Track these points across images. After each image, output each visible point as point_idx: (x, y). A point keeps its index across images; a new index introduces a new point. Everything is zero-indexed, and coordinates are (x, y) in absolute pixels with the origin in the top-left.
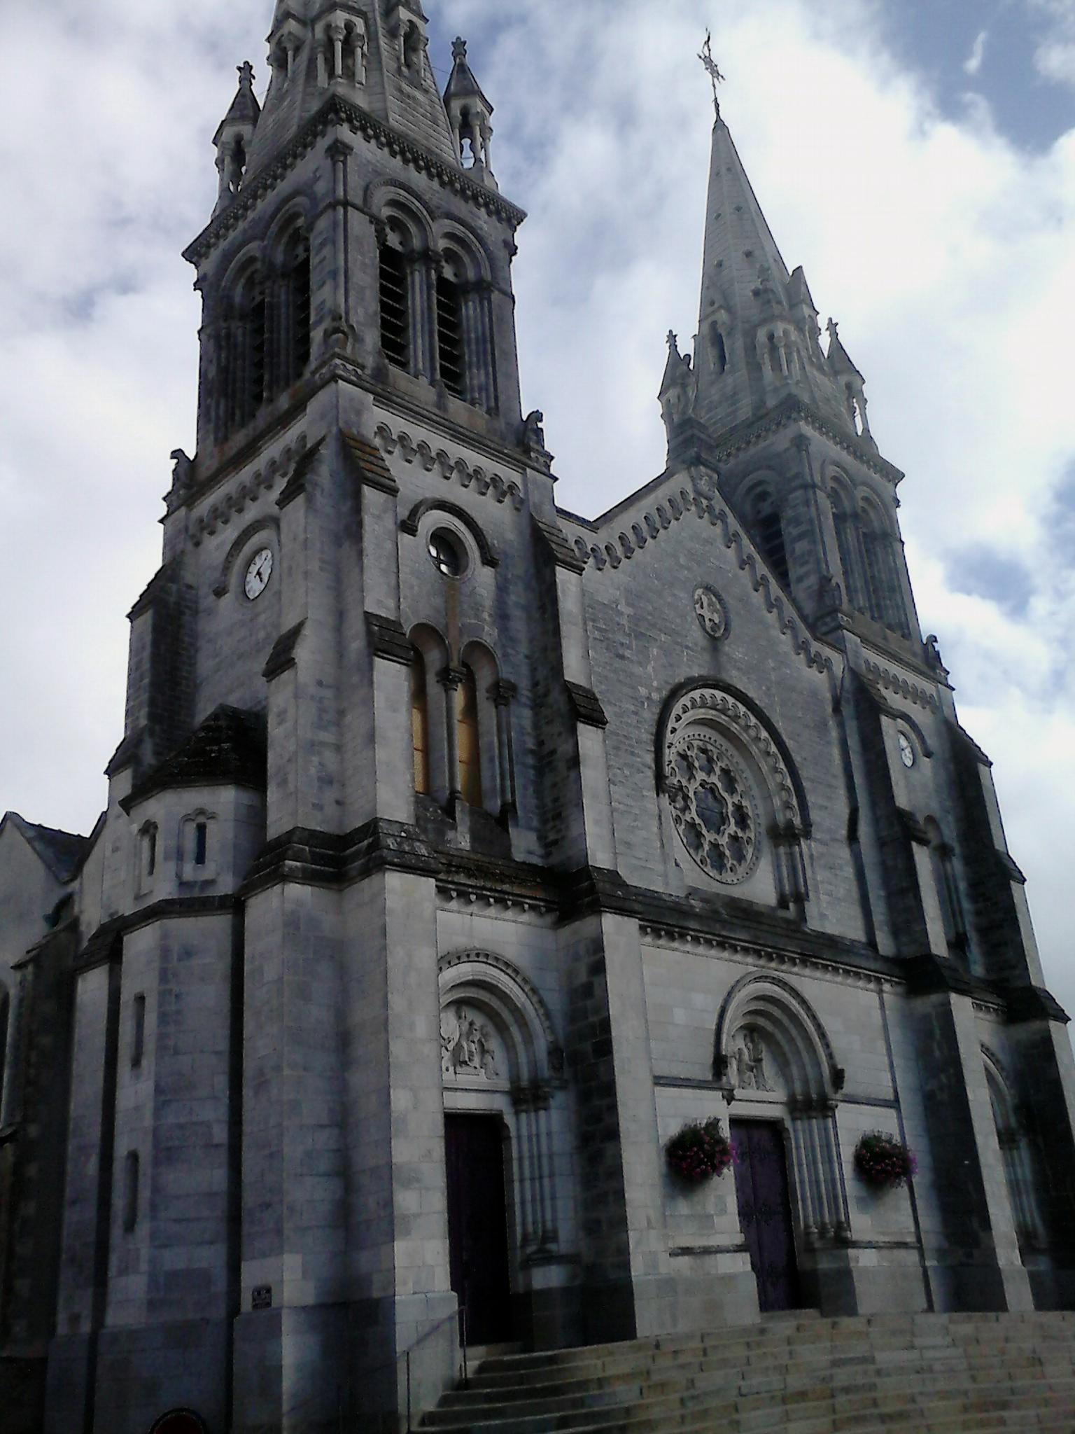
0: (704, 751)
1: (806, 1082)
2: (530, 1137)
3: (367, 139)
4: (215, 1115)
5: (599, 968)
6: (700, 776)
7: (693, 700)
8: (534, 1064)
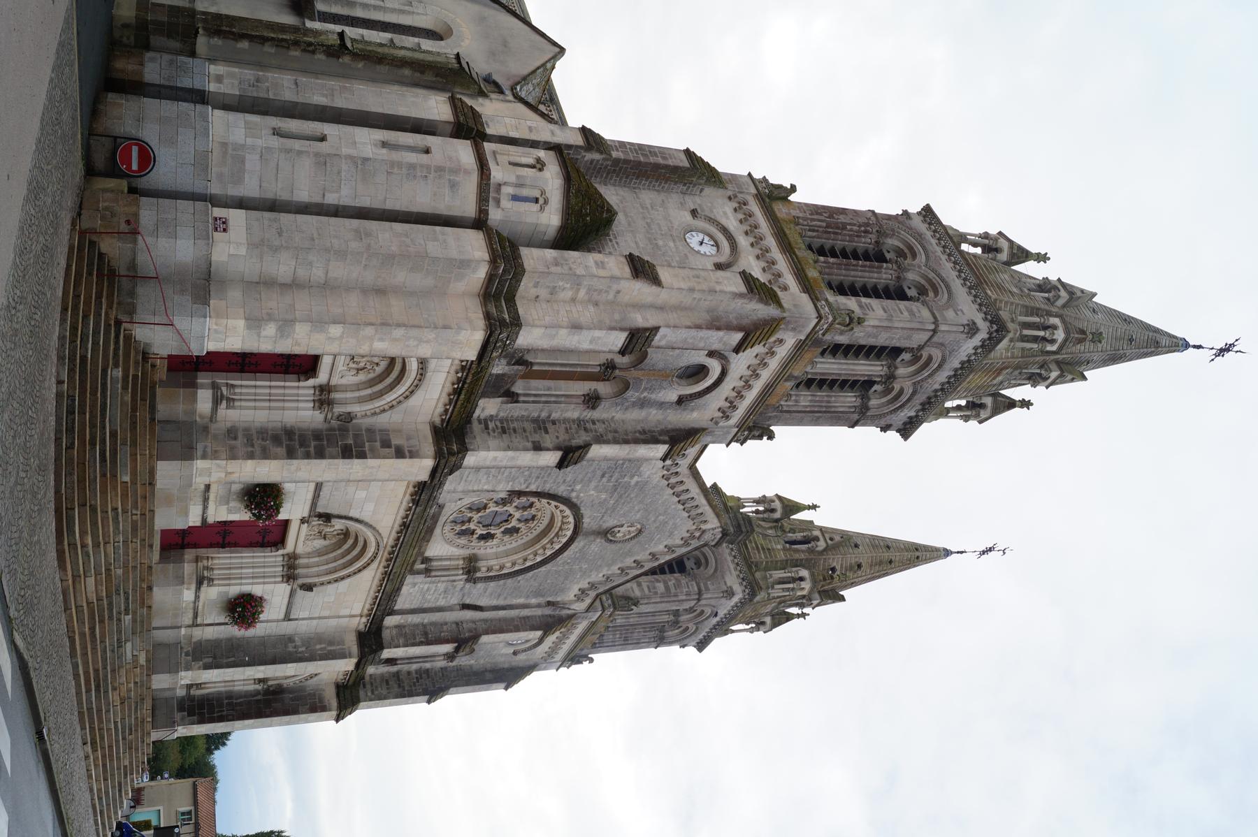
0: (533, 518)
1: (307, 566)
2: (298, 395)
3: (976, 348)
4: (343, 196)
5: (400, 454)
6: (517, 515)
7: (567, 517)
8: (344, 403)
